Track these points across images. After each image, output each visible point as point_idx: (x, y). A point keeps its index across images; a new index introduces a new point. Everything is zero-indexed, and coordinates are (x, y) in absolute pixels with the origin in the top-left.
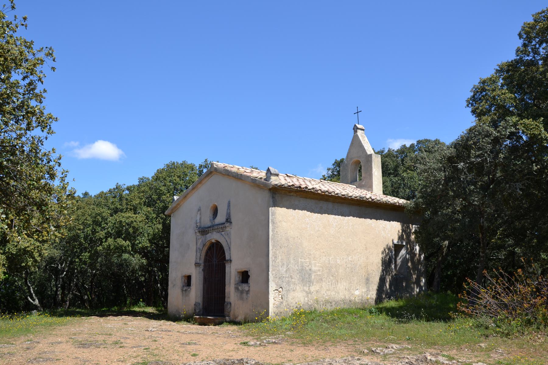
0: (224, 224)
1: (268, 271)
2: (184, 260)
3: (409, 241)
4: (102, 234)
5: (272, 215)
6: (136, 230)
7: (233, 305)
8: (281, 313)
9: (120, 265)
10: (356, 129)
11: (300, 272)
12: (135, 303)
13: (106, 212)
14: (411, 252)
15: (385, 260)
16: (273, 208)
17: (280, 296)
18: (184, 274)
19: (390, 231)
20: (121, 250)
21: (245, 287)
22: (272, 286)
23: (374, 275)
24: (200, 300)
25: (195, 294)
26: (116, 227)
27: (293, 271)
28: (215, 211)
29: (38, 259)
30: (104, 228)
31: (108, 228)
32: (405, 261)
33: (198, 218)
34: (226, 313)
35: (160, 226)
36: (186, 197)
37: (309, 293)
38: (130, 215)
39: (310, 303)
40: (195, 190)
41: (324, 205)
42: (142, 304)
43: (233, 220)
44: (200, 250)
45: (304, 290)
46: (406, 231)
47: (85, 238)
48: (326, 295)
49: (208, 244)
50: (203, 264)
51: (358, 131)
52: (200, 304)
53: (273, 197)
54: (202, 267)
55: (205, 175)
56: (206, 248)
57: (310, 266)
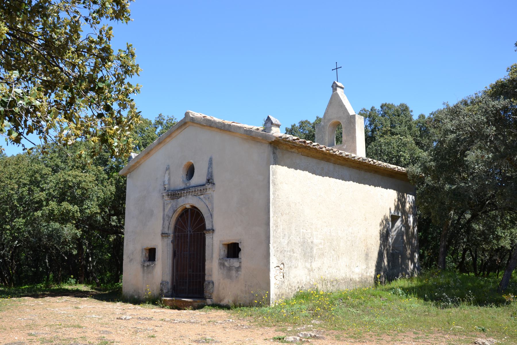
0: (204, 185)
1: (269, 243)
2: (146, 229)
3: (404, 212)
5: (273, 175)
7: (216, 284)
8: (282, 294)
9: (50, 236)
11: (302, 245)
12: (65, 280)
14: (406, 224)
15: (383, 233)
16: (274, 166)
17: (282, 274)
18: (145, 247)
19: (385, 199)
21: (234, 262)
22: (274, 261)
23: (372, 250)
24: (168, 278)
25: (162, 271)
26: (60, 188)
27: (295, 244)
28: (191, 171)
30: (42, 190)
31: (49, 189)
32: (400, 234)
33: (166, 179)
34: (207, 294)
35: (113, 189)
36: (148, 153)
37: (311, 270)
38: (76, 173)
39: (312, 283)
40: (162, 145)
42: (73, 281)
43: (216, 181)
44: (169, 217)
45: (306, 267)
46: (401, 202)
47: (20, 199)
48: (327, 272)
49: (179, 210)
50: (172, 235)
51: (338, 89)
52: (168, 283)
53: (274, 153)
54: (171, 238)
55: (177, 127)
56: (176, 215)
57: (312, 238)
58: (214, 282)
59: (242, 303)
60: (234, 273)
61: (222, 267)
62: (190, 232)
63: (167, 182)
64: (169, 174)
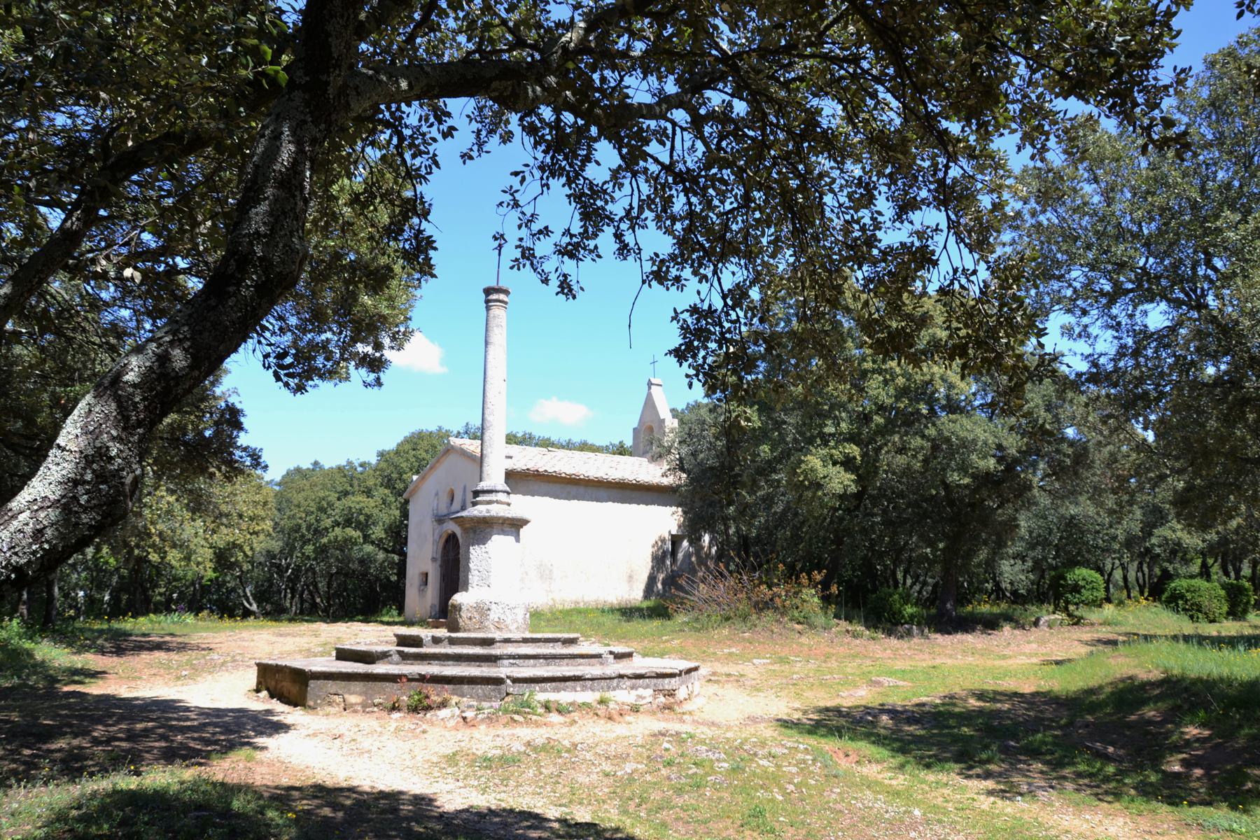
4: (328, 522)
6: (368, 517)
9: (362, 561)
10: (650, 384)
13: (333, 497)
19: (667, 520)
20: (349, 541)
29: (250, 553)
32: (688, 555)
41: (573, 489)
47: (308, 528)
49: (445, 537)
54: (439, 562)
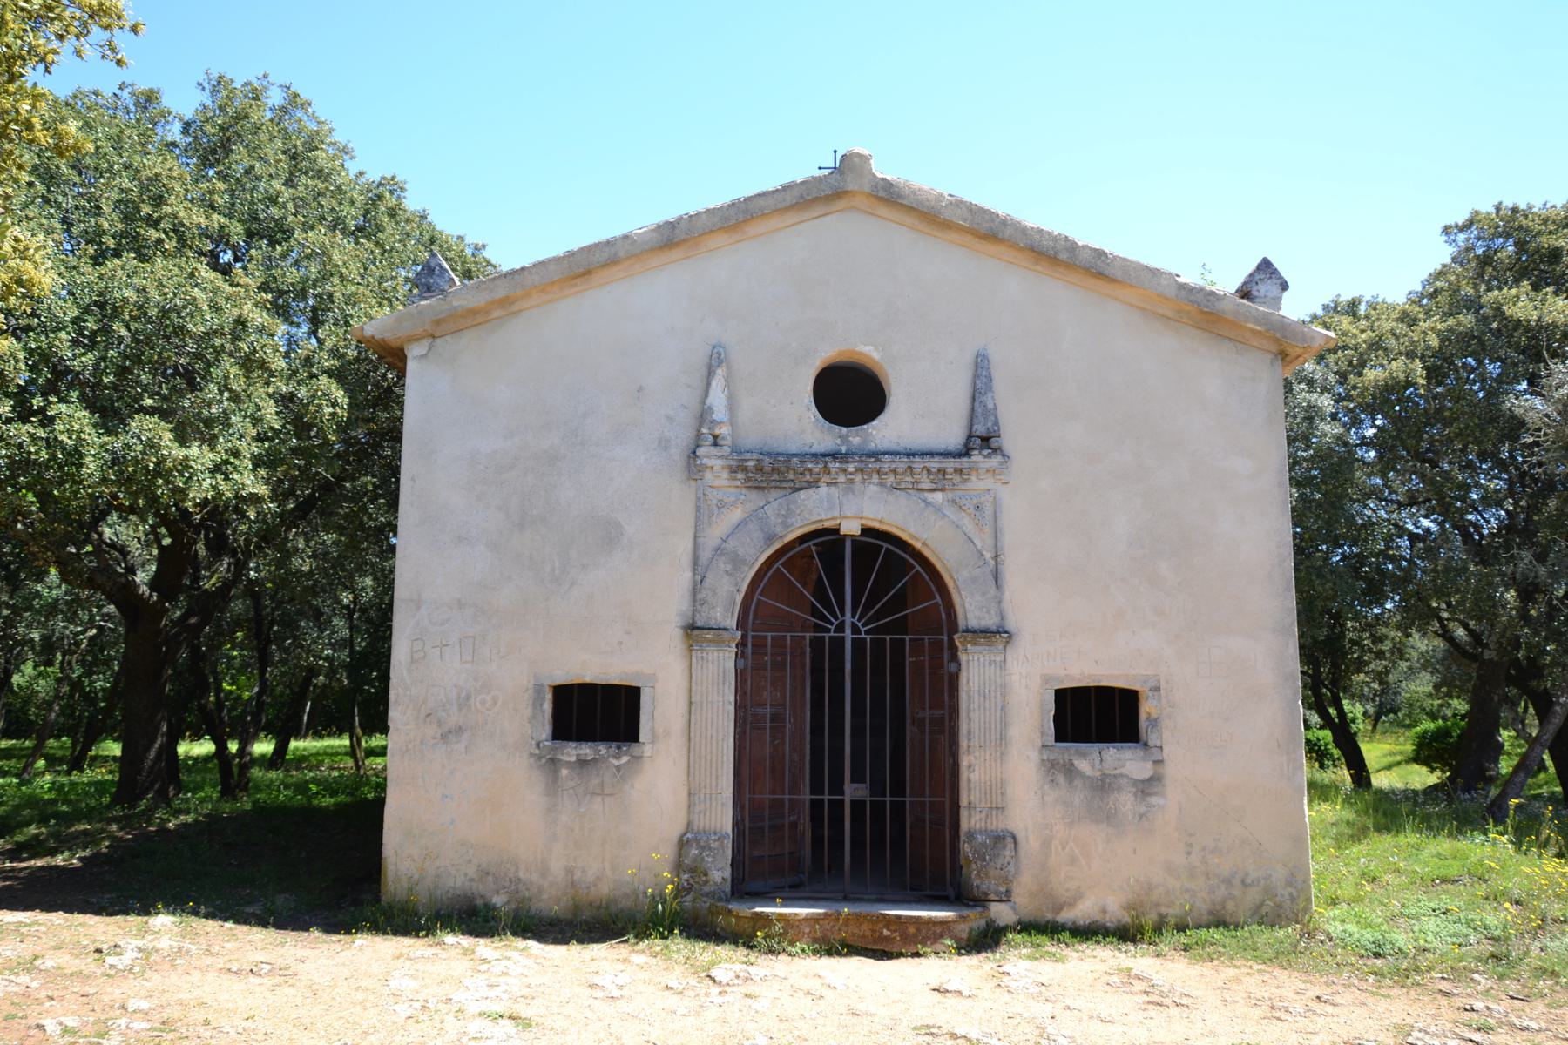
7: (1030, 843)
25: (676, 789)
40: (677, 253)
58: (1020, 836)
59: (1173, 913)
60: (1126, 801)
61: (1061, 778)
62: (855, 630)
63: (720, 413)
64: (728, 381)
